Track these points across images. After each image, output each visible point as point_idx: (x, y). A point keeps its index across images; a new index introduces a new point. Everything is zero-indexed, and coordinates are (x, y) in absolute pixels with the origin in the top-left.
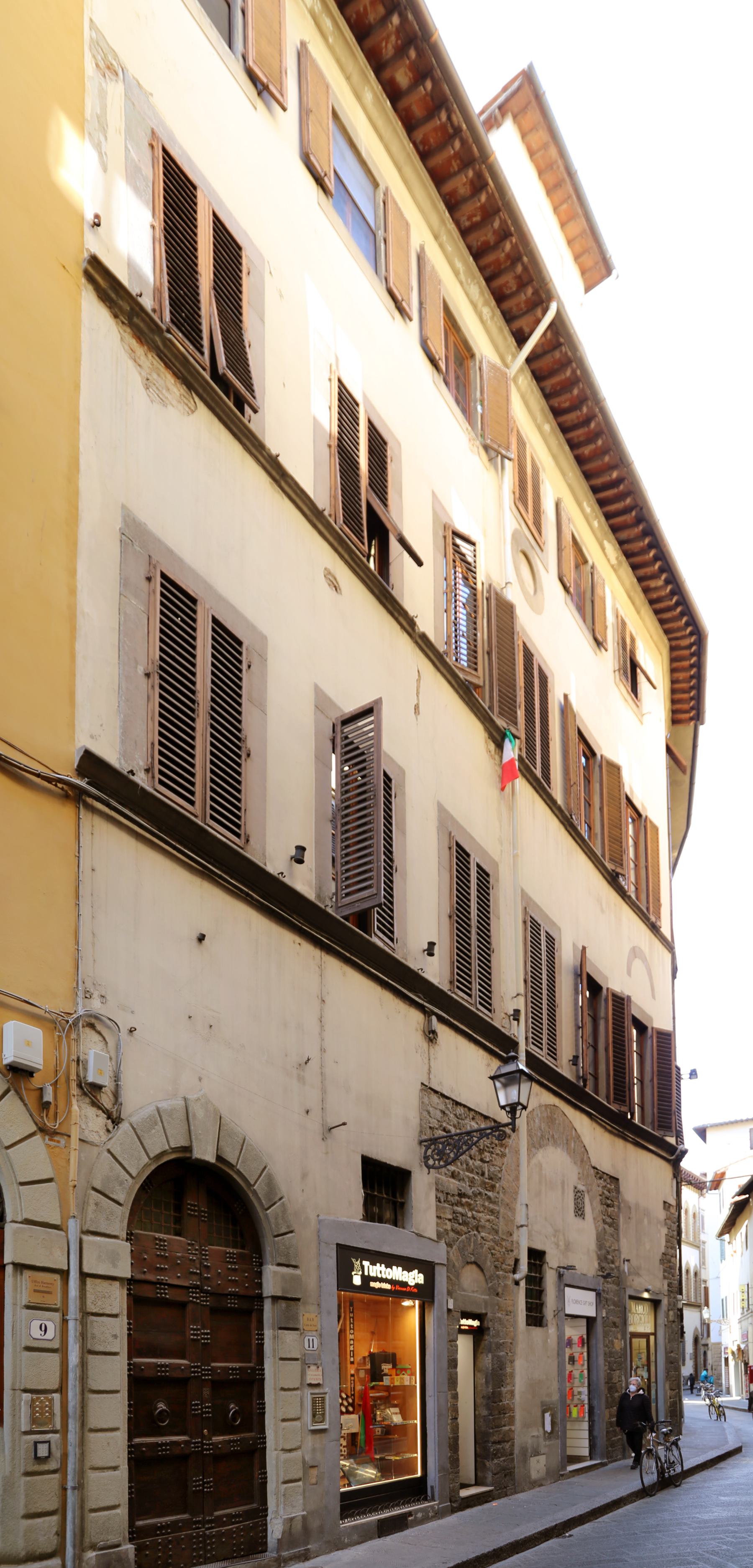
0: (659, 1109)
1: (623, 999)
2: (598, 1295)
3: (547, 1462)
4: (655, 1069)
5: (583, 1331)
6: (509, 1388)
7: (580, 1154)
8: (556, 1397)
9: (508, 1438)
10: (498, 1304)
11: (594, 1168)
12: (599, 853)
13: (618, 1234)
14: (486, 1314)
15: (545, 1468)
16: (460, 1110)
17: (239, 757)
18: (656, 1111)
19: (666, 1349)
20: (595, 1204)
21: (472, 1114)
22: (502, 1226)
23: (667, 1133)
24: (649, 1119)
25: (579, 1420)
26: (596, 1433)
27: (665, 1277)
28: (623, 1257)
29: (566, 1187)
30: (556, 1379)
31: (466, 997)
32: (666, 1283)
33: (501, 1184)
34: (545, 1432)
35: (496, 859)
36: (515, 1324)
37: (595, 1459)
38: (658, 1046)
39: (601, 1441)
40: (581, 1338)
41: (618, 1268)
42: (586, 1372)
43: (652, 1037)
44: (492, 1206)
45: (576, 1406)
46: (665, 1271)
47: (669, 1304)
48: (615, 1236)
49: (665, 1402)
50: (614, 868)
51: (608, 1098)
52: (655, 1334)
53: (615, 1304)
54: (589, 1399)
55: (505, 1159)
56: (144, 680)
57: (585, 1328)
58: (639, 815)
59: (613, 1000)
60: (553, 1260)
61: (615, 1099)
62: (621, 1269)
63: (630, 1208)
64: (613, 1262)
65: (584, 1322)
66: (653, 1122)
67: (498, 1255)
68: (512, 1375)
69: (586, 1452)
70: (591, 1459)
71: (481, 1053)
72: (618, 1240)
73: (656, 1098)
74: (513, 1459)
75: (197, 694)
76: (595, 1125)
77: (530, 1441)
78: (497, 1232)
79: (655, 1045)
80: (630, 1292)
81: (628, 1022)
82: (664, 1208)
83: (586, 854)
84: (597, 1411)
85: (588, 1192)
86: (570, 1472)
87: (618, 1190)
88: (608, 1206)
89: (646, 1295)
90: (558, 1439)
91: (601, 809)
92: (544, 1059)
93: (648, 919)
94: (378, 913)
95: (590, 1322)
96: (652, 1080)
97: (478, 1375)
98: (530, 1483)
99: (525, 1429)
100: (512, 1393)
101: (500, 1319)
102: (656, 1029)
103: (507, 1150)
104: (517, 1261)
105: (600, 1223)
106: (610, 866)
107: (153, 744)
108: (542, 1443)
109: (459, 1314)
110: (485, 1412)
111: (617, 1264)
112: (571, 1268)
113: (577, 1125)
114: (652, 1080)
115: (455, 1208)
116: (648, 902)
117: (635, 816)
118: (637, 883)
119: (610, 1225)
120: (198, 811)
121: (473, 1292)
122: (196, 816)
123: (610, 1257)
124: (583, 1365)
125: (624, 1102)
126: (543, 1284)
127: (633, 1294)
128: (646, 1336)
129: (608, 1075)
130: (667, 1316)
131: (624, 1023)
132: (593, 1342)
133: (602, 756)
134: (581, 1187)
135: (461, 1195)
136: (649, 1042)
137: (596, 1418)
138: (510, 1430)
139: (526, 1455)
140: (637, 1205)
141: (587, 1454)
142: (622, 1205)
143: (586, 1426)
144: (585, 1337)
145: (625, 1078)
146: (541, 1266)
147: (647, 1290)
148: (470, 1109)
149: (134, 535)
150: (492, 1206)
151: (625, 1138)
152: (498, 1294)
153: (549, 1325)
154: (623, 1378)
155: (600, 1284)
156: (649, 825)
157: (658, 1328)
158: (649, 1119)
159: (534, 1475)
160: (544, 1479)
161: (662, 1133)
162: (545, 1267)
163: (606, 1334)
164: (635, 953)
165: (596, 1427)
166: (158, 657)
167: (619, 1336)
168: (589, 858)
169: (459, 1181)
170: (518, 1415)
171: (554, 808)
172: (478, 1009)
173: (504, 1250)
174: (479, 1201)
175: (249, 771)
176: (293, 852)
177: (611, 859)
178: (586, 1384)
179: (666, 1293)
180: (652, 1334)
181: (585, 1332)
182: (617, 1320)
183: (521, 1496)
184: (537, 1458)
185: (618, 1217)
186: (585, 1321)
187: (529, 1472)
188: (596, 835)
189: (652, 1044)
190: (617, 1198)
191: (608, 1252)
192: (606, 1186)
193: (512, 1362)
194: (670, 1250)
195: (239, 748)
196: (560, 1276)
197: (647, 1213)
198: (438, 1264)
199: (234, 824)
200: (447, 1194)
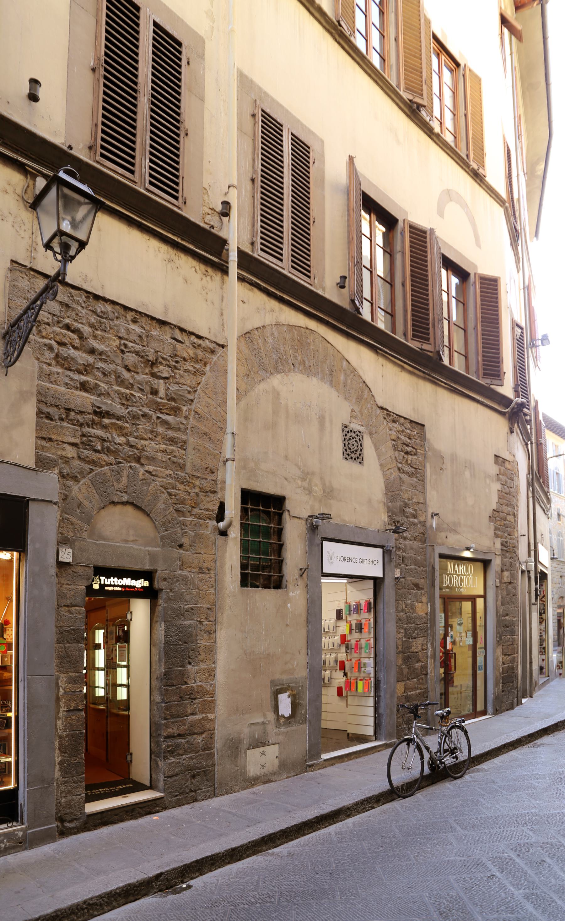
0: (483, 356)
1: (425, 232)
2: (387, 552)
3: (280, 753)
4: (479, 315)
5: (369, 595)
6: (203, 666)
7: (361, 392)
8: (301, 673)
9: (206, 729)
10: (180, 559)
11: (382, 408)
12: (394, 83)
13: (424, 486)
14: (156, 571)
15: (276, 761)
16: (100, 307)
17: (178, 135)
18: (480, 358)
19: (497, 612)
20: (383, 448)
21: (130, 315)
22: (191, 458)
23: (494, 382)
24: (473, 368)
25: (364, 695)
26: (381, 711)
27: (496, 536)
28: (430, 511)
29: (327, 424)
30: (304, 651)
31: (275, 260)
32: (498, 542)
33: (193, 407)
34: (278, 717)
35: (202, 33)
36: (217, 585)
37: (380, 740)
38: (481, 292)
39: (388, 722)
40: (369, 604)
41: (424, 524)
42: (372, 641)
43: (475, 283)
44: (171, 434)
45: (361, 680)
46: (496, 529)
47: (503, 564)
48: (419, 487)
49: (495, 668)
50: (411, 97)
51: (405, 335)
52: (484, 597)
53: (416, 563)
54: (375, 672)
55: (204, 379)
56: (90, 73)
57: (372, 591)
58: (458, 65)
59: (410, 232)
60: (299, 506)
61: (414, 336)
62: (428, 524)
63: (442, 458)
64: (415, 517)
65: (371, 583)
66: (477, 372)
67: (182, 495)
68: (211, 650)
69: (370, 731)
70: (376, 739)
71: (154, 243)
72: (424, 493)
73: (480, 345)
74: (212, 755)
75: (139, 85)
76: (381, 360)
77: (246, 730)
78: (182, 467)
79: (478, 290)
80: (439, 550)
81: (435, 262)
82: (496, 462)
83: (370, 76)
84: (383, 686)
85: (371, 434)
86: (325, 760)
87: (423, 437)
88: (407, 453)
89: (467, 554)
90: (304, 722)
91: (396, 40)
92: (285, 272)
93: (468, 166)
94: (521, 388)
95: (377, 582)
96: (476, 328)
97: (153, 649)
98: (245, 781)
99: (227, 717)
100: (211, 673)
101: (185, 579)
102: (479, 274)
103: (208, 368)
104: (222, 506)
105: (395, 474)
106: (406, 96)
107: (96, 125)
108: (272, 729)
109: (91, 571)
110: (158, 698)
111: (422, 519)
112: (327, 517)
113: (354, 362)
114: (476, 328)
115: (86, 430)
116: (468, 149)
117: (452, 65)
118: (455, 132)
119: (411, 475)
120: (285, 267)
121: (126, 541)
122: (284, 269)
123: (409, 510)
124: (370, 633)
125: (428, 339)
126: (283, 538)
127: (446, 552)
128: (473, 599)
129: (405, 311)
130: (501, 577)
131: (426, 257)
132: (380, 606)
133: (465, 65)
134: (355, 426)
135: (100, 413)
136: (472, 289)
137: (382, 694)
138: (205, 719)
139: (235, 747)
140: (454, 458)
141: (372, 733)
142: (430, 453)
143: (371, 702)
144: (372, 601)
145: (428, 315)
146: (280, 515)
147: (468, 549)
148: (126, 308)
149: (245, 83)
150: (171, 434)
151: (434, 382)
152: (181, 546)
153: (291, 586)
154: (429, 646)
155: (391, 540)
156: (468, 73)
157: (488, 590)
158: (473, 368)
159: (253, 770)
160: (274, 774)
161: (488, 381)
162: (286, 516)
163: (399, 598)
164: (448, 195)
165: (382, 704)
166: (103, 53)
167: (424, 599)
168: (376, 82)
169: (99, 395)
170: (221, 700)
171: (312, 9)
172: (148, 191)
173: (197, 490)
174: (143, 425)
175: (187, 147)
176: (338, 280)
177: (406, 88)
178: (372, 655)
179: (499, 552)
180: (480, 596)
181: (372, 595)
182: (421, 582)
183: (215, 802)
184: (261, 749)
185: (425, 467)
186: (372, 582)
187: (245, 767)
188: (390, 67)
189: (474, 291)
190: (423, 446)
191: (407, 505)
192: (403, 431)
193: (210, 633)
194: (504, 507)
195: (178, 128)
196: (313, 528)
197: (469, 465)
198: (34, 500)
199: (306, 270)
200: (68, 410)
